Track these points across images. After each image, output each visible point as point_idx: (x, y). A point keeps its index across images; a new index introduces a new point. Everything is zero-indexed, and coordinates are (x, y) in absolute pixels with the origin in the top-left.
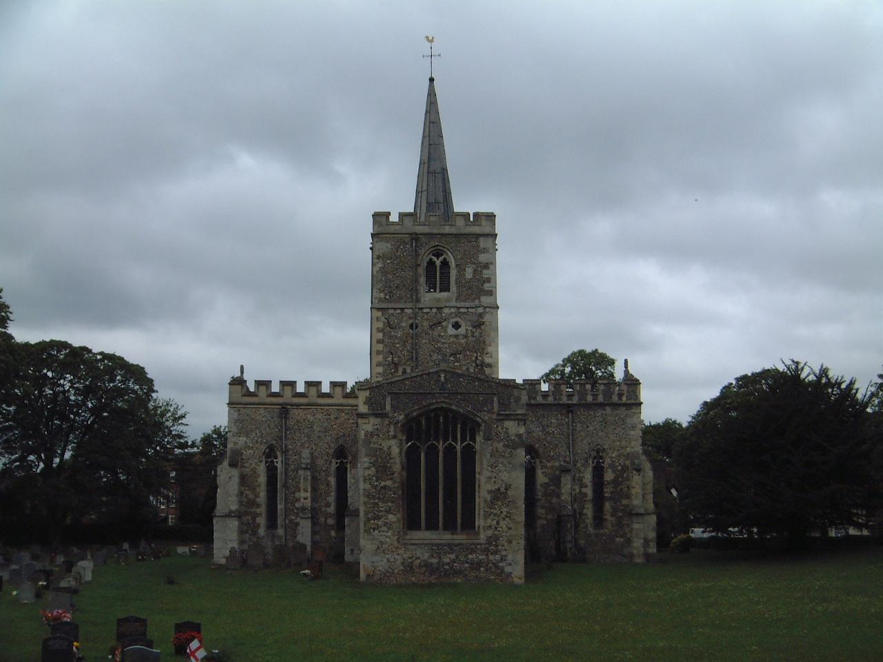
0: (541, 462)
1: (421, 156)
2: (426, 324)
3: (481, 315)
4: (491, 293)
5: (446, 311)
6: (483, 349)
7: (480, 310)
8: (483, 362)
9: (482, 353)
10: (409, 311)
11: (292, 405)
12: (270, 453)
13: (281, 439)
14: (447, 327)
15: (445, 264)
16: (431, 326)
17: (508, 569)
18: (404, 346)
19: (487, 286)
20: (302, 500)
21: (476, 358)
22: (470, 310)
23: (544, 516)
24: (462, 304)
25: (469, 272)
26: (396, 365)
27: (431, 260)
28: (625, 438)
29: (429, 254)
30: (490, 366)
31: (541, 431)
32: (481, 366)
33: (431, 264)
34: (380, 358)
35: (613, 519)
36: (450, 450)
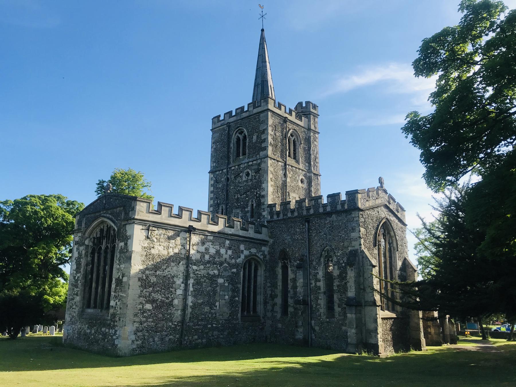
0: (290, 262)
1: (256, 79)
2: (233, 177)
6: (260, 186)
7: (259, 161)
8: (260, 195)
9: (260, 189)
14: (242, 176)
16: (235, 177)
18: (222, 192)
21: (257, 193)
22: (254, 162)
23: (292, 305)
27: (238, 136)
28: (347, 239)
29: (236, 133)
30: (263, 196)
31: (291, 239)
32: (259, 197)
34: (212, 202)
35: (340, 309)
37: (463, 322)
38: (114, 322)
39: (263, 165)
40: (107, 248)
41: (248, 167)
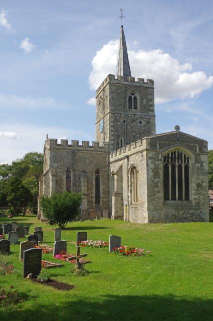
3: (149, 119)
4: (153, 111)
5: (137, 116)
7: (149, 117)
10: (123, 115)
11: (77, 150)
12: (68, 171)
13: (73, 165)
15: (135, 98)
17: (203, 216)
18: (122, 129)
19: (151, 108)
20: (83, 191)
22: (146, 117)
24: (143, 114)
25: (145, 102)
26: (119, 136)
33: (130, 97)
34: (112, 133)
36: (180, 167)
37: (77, 202)
38: (199, 207)
39: (151, 120)
40: (175, 162)
41: (141, 118)
